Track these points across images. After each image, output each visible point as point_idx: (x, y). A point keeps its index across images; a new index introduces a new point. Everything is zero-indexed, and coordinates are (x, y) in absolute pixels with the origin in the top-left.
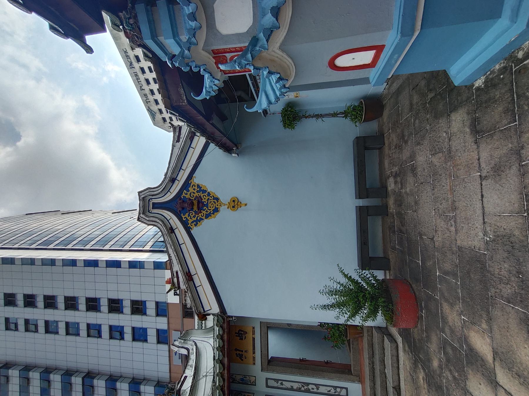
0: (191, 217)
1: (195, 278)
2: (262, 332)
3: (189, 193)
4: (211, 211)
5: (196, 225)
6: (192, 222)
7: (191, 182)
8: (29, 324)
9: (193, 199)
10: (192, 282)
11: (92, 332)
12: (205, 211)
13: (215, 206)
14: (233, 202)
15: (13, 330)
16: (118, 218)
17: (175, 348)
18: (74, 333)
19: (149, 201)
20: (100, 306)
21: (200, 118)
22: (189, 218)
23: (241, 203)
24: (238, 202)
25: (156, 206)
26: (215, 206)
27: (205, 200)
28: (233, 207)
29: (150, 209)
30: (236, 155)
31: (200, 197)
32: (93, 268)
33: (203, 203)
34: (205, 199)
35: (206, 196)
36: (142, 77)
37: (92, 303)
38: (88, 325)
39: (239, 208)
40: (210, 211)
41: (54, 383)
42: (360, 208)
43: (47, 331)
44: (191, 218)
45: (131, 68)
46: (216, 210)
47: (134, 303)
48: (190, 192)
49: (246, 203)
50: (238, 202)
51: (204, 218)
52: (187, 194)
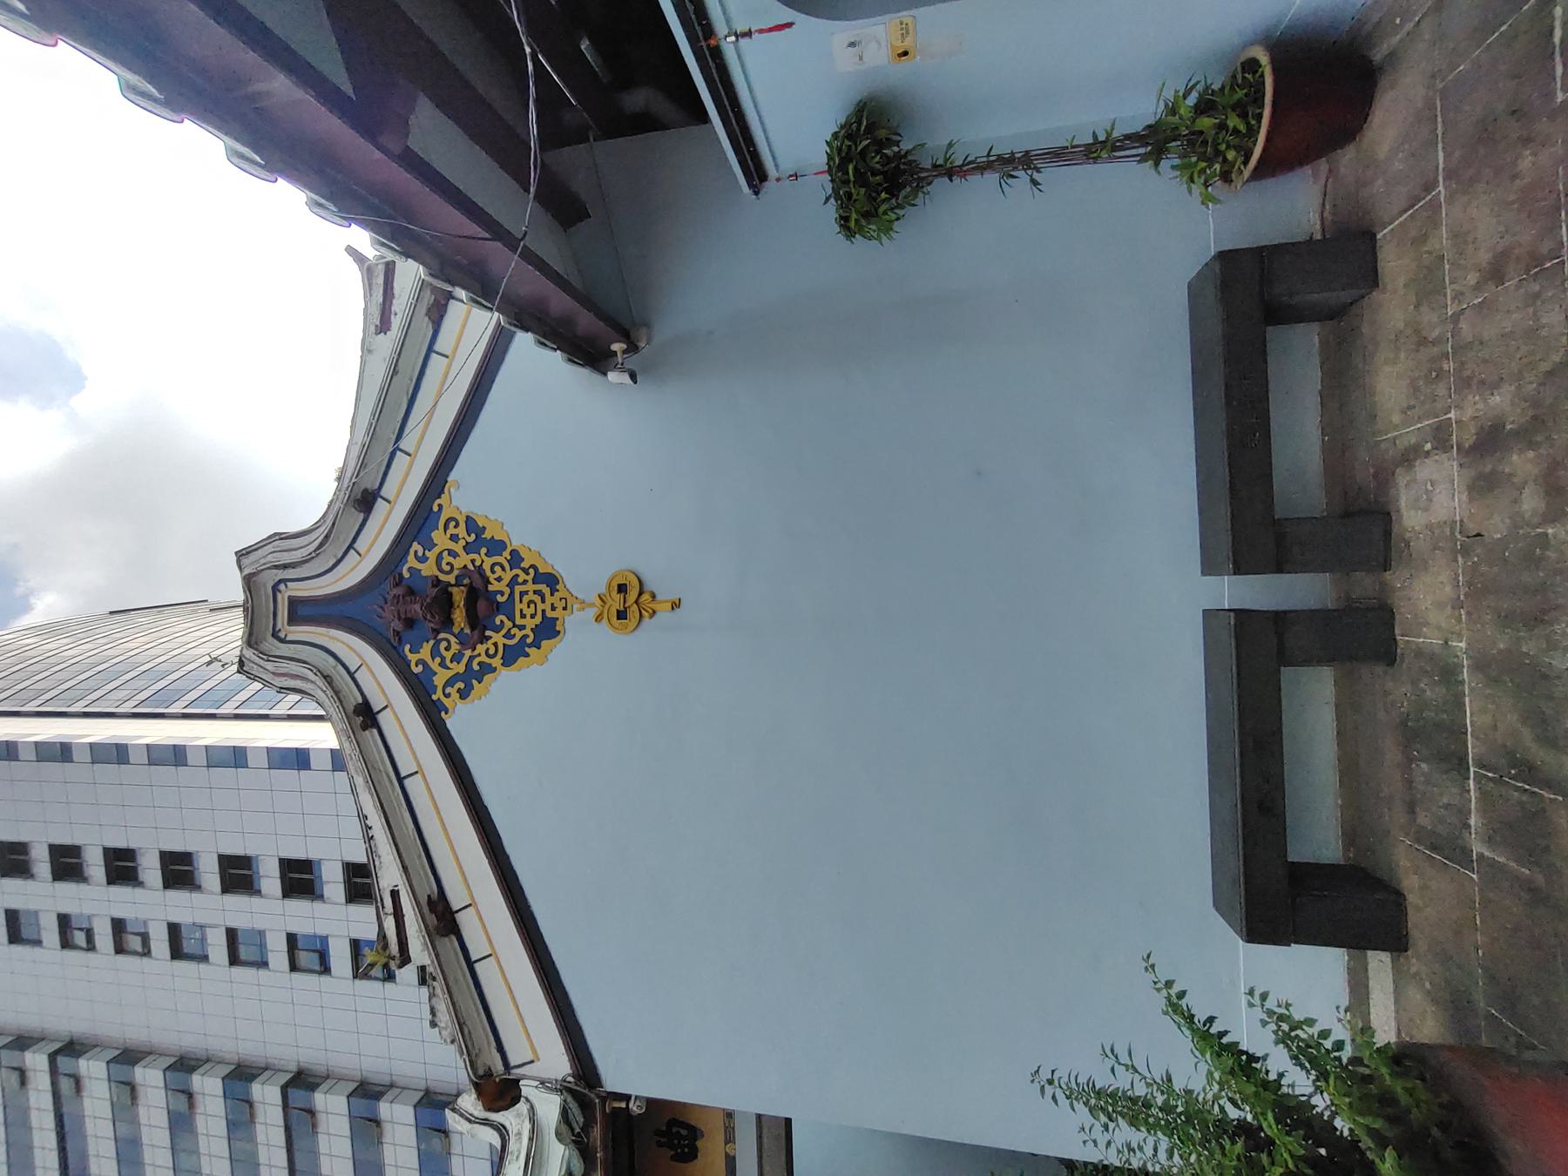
0: (443, 659)
1: (466, 921)
2: (765, 1131)
3: (432, 555)
4: (527, 631)
5: (464, 695)
6: (450, 682)
7: (440, 506)
8: (127, 932)
9: (451, 579)
10: (454, 938)
11: (304, 958)
12: (504, 632)
13: (543, 611)
14: (525, 615)
15: (81, 948)
17: (458, 1123)
18: (252, 959)
19: (275, 589)
21: (331, 126)
22: (435, 665)
23: (653, 596)
24: (641, 594)
25: (302, 611)
26: (543, 611)
27: (502, 586)
28: (621, 615)
29: (279, 626)
30: (626, 379)
31: (480, 569)
32: (296, 771)
33: (490, 597)
34: (499, 579)
35: (503, 569)
37: (297, 876)
38: (292, 939)
39: (646, 620)
40: (524, 632)
41: (204, 1098)
42: (1243, 618)
43: (177, 953)
44: (443, 665)
46: (548, 629)
48: (436, 550)
49: (675, 597)
50: (641, 594)
51: (496, 662)
52: (423, 559)
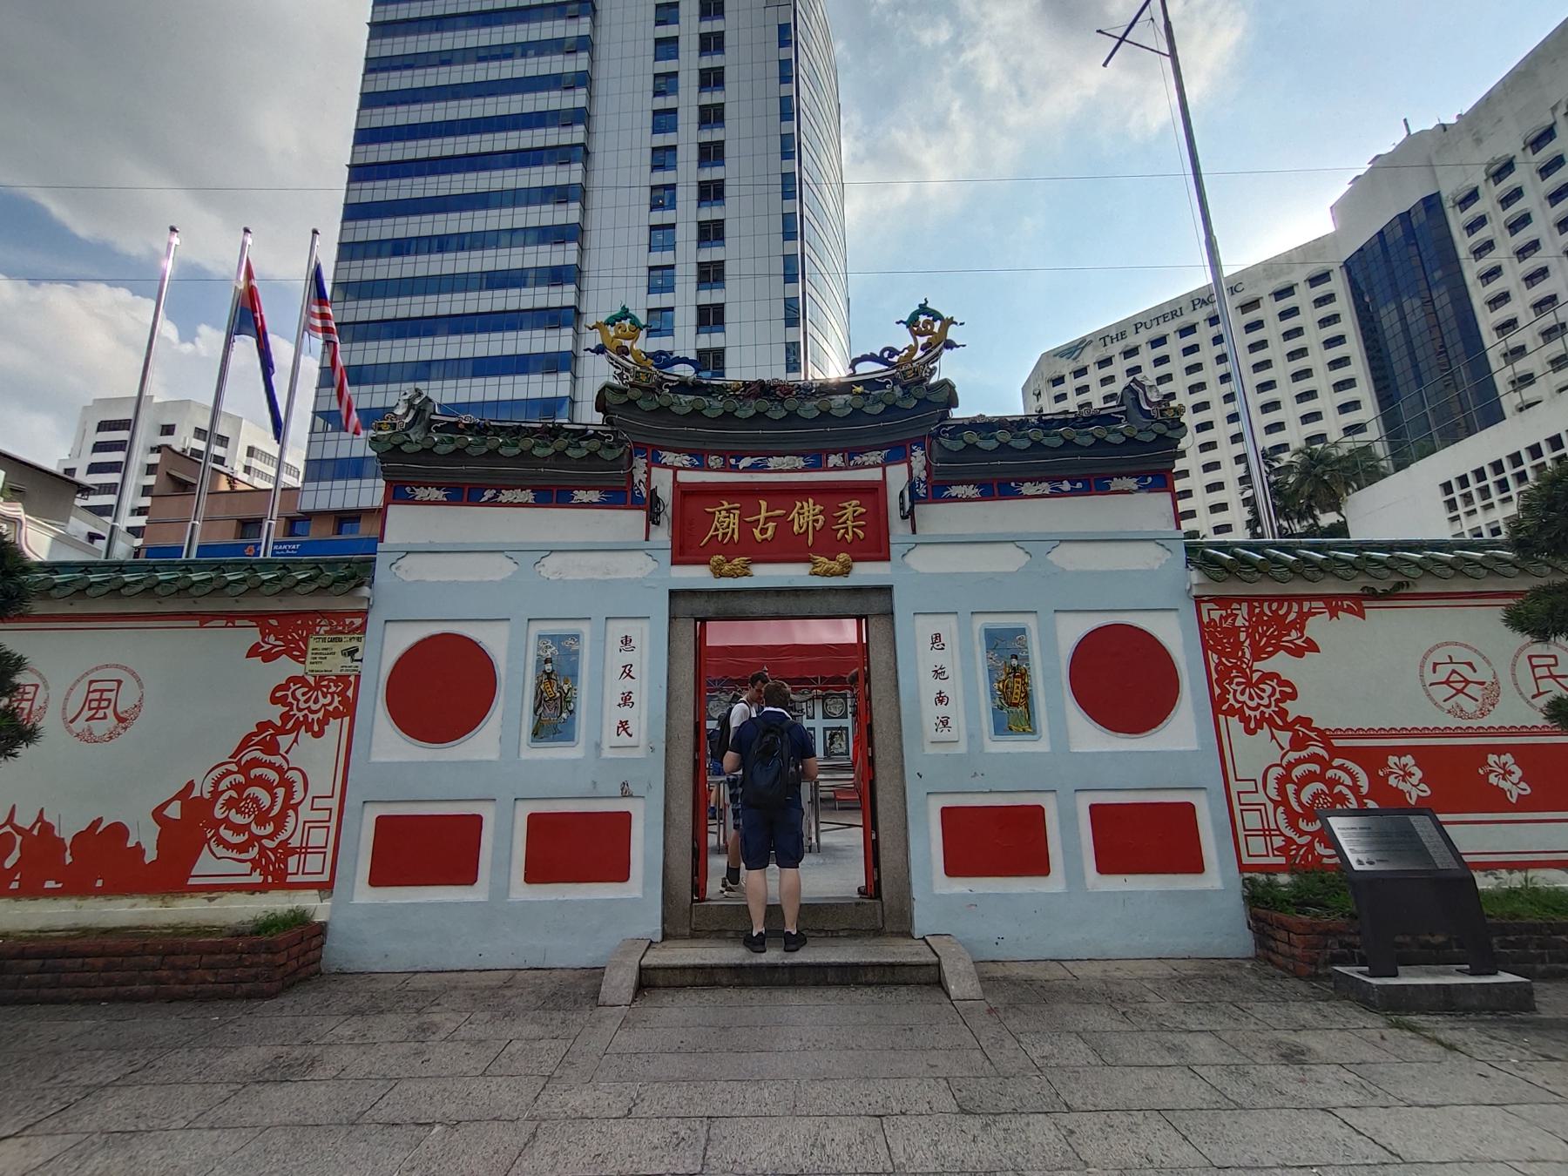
16: (835, 292)
36: (1169, 328)
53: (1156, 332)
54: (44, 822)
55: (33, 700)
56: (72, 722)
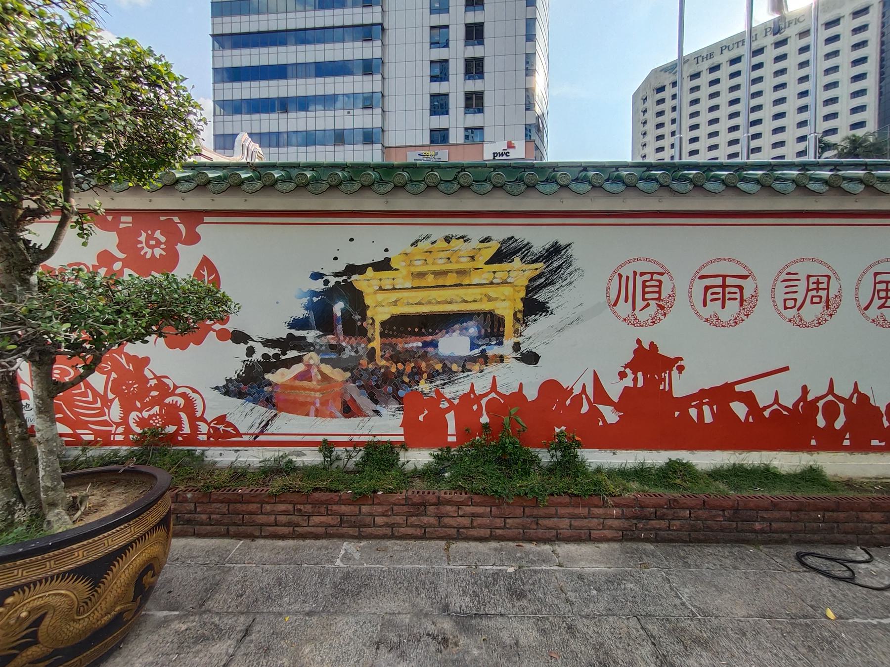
20: (474, 45)
45: (766, 29)
47: (480, 95)
53: (734, 54)
54: (859, 393)
55: (828, 289)
56: (866, 308)
